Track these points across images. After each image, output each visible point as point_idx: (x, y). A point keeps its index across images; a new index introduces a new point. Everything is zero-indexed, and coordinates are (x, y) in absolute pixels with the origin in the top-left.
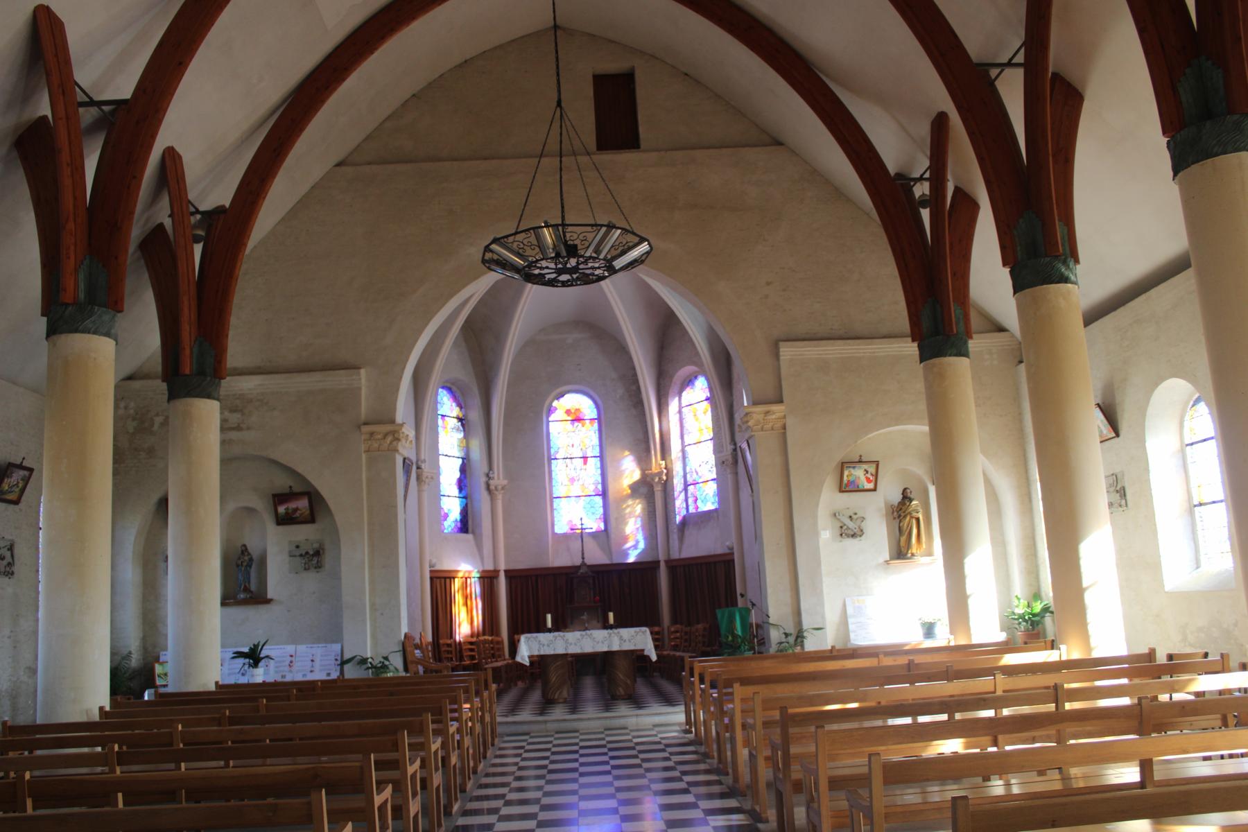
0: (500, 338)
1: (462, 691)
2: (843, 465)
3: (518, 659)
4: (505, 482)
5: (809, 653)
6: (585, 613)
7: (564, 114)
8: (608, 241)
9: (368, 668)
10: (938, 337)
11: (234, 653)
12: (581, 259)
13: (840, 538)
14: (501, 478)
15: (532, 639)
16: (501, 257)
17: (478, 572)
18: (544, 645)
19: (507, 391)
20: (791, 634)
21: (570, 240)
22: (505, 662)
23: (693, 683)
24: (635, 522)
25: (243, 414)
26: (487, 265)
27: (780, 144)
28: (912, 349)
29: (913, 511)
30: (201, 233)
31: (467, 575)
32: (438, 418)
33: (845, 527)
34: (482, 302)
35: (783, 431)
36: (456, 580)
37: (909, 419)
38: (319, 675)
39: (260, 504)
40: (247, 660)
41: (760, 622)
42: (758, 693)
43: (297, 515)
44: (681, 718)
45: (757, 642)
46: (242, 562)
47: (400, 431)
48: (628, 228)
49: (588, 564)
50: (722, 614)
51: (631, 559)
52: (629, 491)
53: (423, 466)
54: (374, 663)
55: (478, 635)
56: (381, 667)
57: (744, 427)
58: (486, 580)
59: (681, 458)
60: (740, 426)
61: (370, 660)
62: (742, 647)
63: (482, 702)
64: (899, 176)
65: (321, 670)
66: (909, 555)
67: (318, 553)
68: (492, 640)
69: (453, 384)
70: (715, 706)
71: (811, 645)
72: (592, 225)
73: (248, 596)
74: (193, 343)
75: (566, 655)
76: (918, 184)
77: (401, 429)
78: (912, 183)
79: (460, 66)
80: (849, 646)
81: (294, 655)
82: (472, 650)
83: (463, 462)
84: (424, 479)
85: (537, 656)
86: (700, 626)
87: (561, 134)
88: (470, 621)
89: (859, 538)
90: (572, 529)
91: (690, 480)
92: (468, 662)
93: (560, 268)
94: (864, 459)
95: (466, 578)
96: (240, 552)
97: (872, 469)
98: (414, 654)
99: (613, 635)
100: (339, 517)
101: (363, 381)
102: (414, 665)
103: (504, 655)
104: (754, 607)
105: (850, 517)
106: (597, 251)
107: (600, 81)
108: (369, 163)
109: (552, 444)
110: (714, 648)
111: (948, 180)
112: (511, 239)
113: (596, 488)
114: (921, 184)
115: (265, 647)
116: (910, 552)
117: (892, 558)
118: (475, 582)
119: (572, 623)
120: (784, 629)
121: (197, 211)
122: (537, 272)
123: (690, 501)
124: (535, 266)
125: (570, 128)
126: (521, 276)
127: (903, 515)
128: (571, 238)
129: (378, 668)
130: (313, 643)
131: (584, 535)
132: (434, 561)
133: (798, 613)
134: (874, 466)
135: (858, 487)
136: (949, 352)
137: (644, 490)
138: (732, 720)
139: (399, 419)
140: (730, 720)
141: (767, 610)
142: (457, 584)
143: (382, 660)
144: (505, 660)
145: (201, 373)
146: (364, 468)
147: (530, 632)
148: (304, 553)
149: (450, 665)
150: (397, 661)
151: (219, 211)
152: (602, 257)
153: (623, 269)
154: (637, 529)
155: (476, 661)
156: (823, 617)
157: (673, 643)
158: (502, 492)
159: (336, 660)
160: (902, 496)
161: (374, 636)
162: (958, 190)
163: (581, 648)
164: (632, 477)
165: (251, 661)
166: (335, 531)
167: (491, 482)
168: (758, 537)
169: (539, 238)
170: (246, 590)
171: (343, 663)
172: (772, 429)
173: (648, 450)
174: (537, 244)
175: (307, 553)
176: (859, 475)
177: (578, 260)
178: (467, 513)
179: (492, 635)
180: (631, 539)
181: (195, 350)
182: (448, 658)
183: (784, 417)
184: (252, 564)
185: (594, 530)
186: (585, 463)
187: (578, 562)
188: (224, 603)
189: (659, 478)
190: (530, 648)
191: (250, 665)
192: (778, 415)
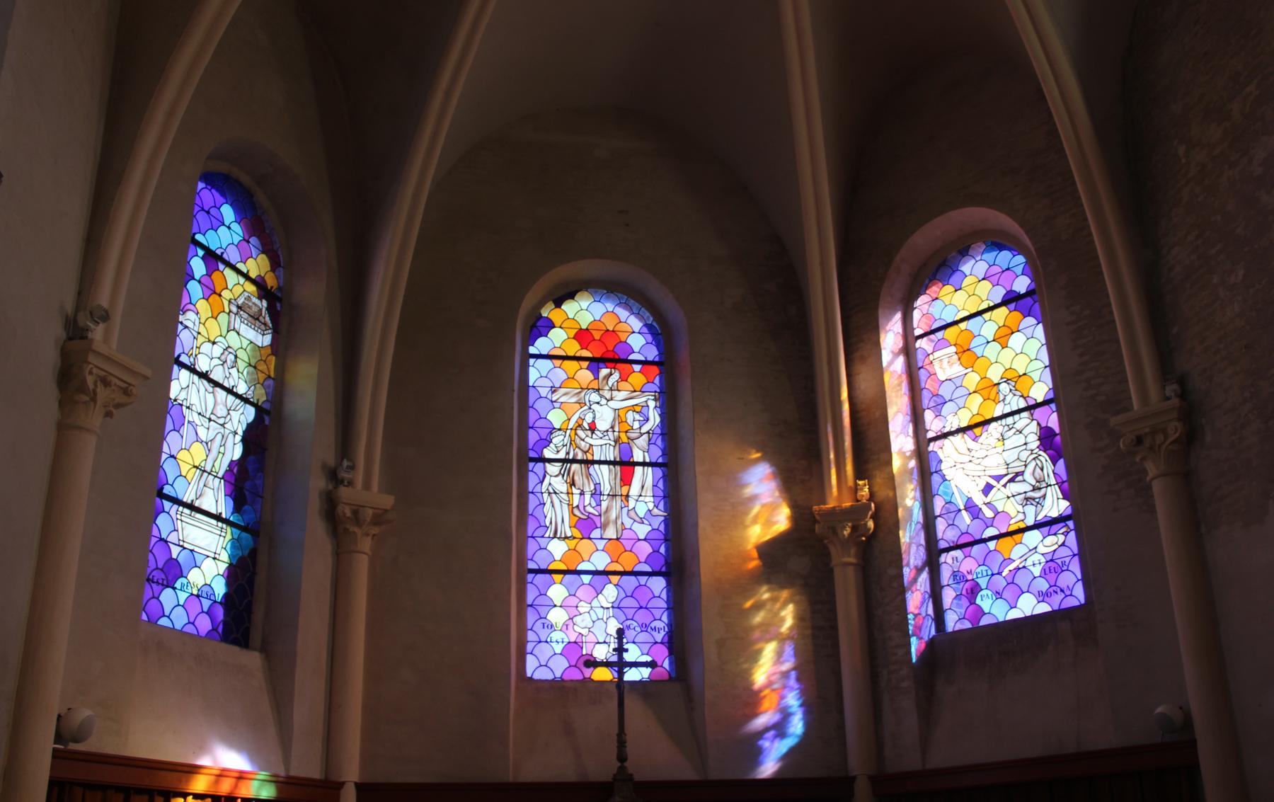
4: (388, 501)
49: (637, 778)
52: (754, 563)
59: (916, 475)
154: (785, 675)
158: (375, 530)
164: (769, 523)
167: (344, 492)
180: (766, 704)
186: (626, 480)
187: (601, 767)
189: (854, 529)
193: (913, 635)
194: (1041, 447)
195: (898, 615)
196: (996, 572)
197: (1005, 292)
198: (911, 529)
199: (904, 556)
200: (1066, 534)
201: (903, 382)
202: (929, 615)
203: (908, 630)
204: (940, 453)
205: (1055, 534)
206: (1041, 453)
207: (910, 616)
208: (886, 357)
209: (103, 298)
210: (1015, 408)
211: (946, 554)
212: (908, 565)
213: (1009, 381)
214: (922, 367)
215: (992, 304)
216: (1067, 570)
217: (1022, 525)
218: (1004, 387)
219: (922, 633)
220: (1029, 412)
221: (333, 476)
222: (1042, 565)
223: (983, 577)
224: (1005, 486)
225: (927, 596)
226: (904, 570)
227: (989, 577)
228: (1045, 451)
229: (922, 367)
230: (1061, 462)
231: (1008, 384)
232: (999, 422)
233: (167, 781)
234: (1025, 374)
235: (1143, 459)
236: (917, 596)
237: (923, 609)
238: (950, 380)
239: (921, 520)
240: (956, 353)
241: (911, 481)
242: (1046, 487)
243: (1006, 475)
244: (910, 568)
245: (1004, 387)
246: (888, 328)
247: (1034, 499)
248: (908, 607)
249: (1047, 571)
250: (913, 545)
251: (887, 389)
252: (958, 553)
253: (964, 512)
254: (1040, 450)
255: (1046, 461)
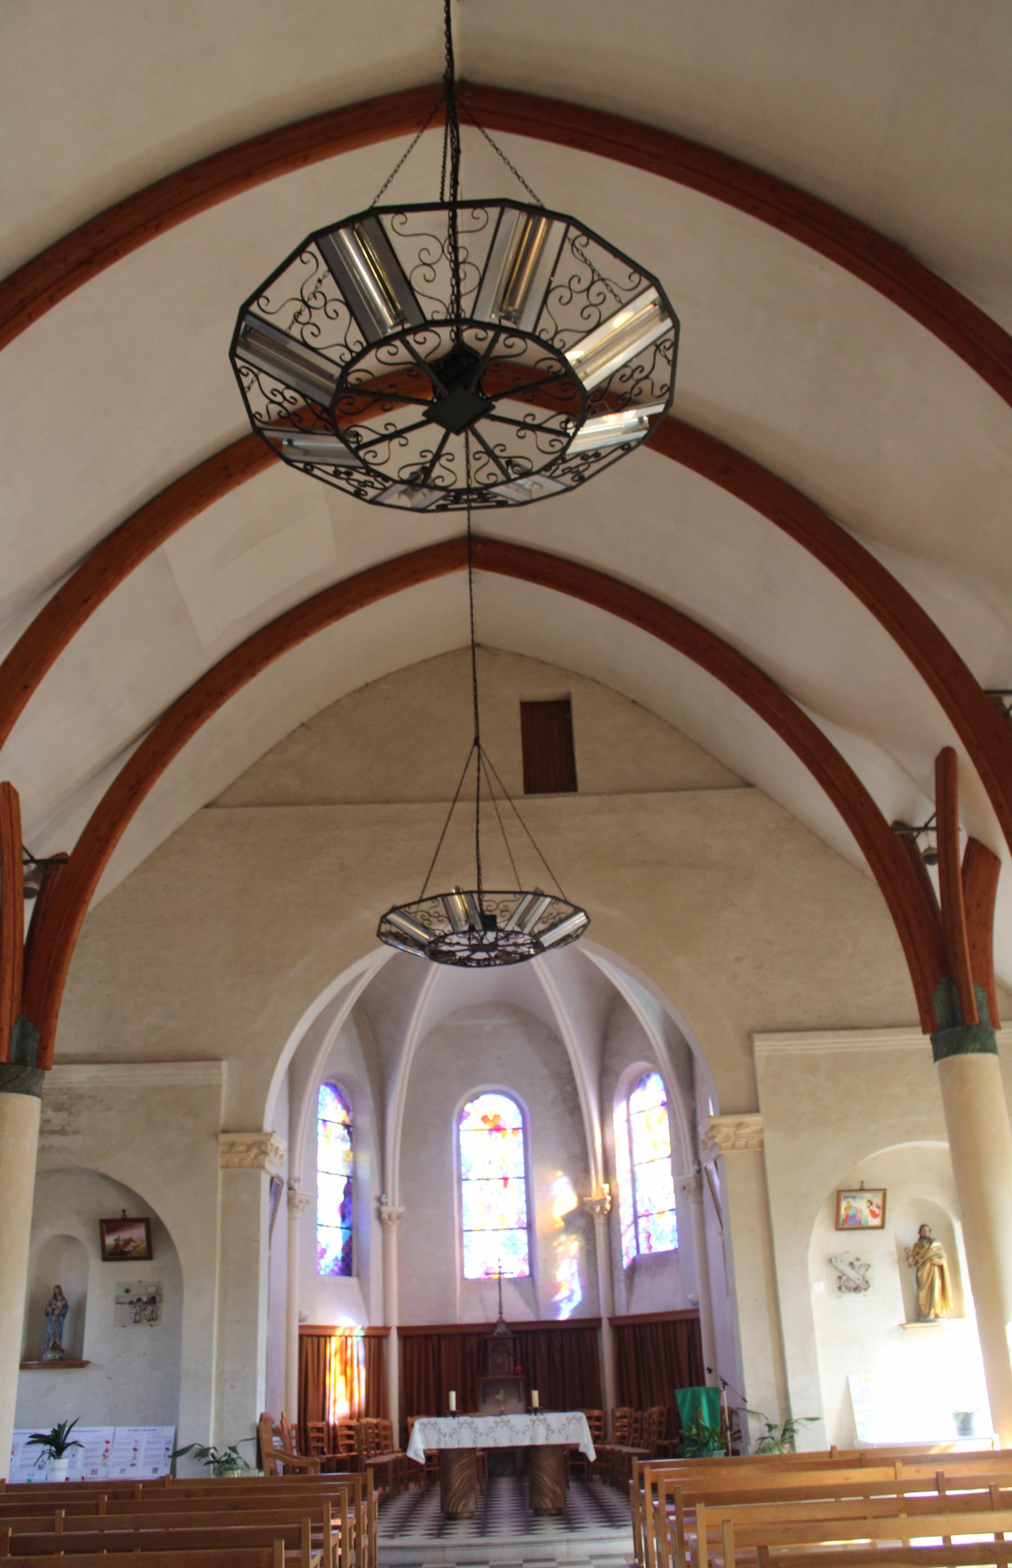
0: (400, 1023)
1: (330, 1504)
2: (839, 1195)
3: (410, 1454)
4: (401, 1209)
5: (802, 1455)
6: (502, 1391)
7: (481, 751)
8: (535, 911)
9: (209, 1462)
10: (955, 1028)
11: (31, 1437)
12: (501, 934)
13: (838, 1293)
14: (397, 1202)
15: (429, 1426)
16: (402, 930)
17: (363, 1329)
18: (445, 1435)
19: (408, 1091)
20: (776, 1427)
21: (488, 910)
22: (393, 1456)
23: (643, 1497)
24: (570, 1265)
25: (70, 1114)
26: (384, 939)
27: (749, 785)
28: (923, 1042)
29: (935, 1255)
30: (35, 886)
31: (347, 1333)
32: (317, 1123)
33: (844, 1278)
34: (379, 977)
35: (760, 1149)
36: (333, 1339)
37: (924, 1133)
38: (142, 1473)
39: (85, 1234)
40: (48, 1447)
41: (734, 1406)
42: (729, 1521)
43: (130, 1248)
44: (628, 1546)
45: (731, 1435)
46: (53, 1309)
47: (269, 1143)
48: (560, 896)
50: (683, 1396)
51: (564, 1315)
52: (562, 1224)
53: (296, 1186)
54: (218, 1456)
55: (359, 1417)
56: (227, 1461)
57: (710, 1143)
58: (372, 1339)
60: (704, 1143)
61: (212, 1451)
62: (711, 1444)
63: (358, 1517)
64: (899, 825)
65: (145, 1464)
66: (932, 1316)
67: (153, 1300)
68: (378, 1423)
69: (339, 1080)
70: (673, 1533)
71: (805, 1443)
72: (515, 893)
73: (57, 1357)
74: (13, 1022)
75: (473, 1450)
76: (922, 835)
77: (270, 1140)
78: (915, 834)
79: (359, 691)
80: (858, 1447)
81: (111, 1441)
82: (350, 1437)
83: (348, 1181)
84: (297, 1203)
85: (437, 1449)
86: (655, 1409)
87: (478, 779)
88: (349, 1395)
89: (863, 1293)
90: (487, 1274)
91: (641, 1210)
92: (344, 1454)
93: (474, 945)
94: (866, 1186)
95: (346, 1337)
96: (52, 1295)
97: (878, 1200)
98: (271, 1442)
99: (537, 1423)
100: (183, 1254)
101: (225, 1076)
102: (270, 1459)
103: (392, 1445)
104: (726, 1387)
105: (851, 1264)
106: (521, 924)
107: (529, 709)
108: (245, 805)
109: (463, 1161)
110: (674, 1441)
111: (959, 829)
112: (414, 908)
113: (520, 1218)
114: (927, 835)
115: (73, 1429)
116: (932, 1312)
117: (909, 1321)
118: (358, 1343)
119: (484, 1402)
120: (767, 1419)
121: (32, 860)
122: (445, 948)
123: (642, 1238)
124: (444, 942)
125: (491, 774)
126: (426, 954)
127: (921, 1261)
128: (489, 908)
129: (223, 1462)
130: (138, 1425)
131: (503, 1283)
132: (305, 1313)
133: (785, 1396)
134: (880, 1194)
135: (860, 1223)
136: (970, 1048)
137: (581, 1223)
138: (695, 1556)
139: (267, 1126)
140: (692, 1557)
141: (743, 1391)
142: (333, 1345)
143: (229, 1451)
144: (393, 1452)
145: (21, 1061)
146: (220, 1190)
147: (428, 1414)
148: (135, 1300)
149: (318, 1460)
150: (248, 1453)
151: (59, 860)
152: (527, 931)
153: (553, 945)
155: (355, 1453)
156: (819, 1402)
157: (618, 1434)
158: (398, 1222)
159: (167, 1449)
160: (918, 1236)
161: (219, 1417)
162: (972, 842)
163: (495, 1441)
165: (53, 1448)
166: (177, 1272)
167: (384, 1209)
168: (730, 1291)
169: (448, 907)
170: (56, 1347)
171: (176, 1454)
172: (746, 1147)
173: (586, 1170)
174: (445, 914)
175: (139, 1300)
176: (860, 1206)
177: (497, 935)
178: (350, 1249)
179: (377, 1416)
181: (16, 1033)
182: (317, 1448)
183: (762, 1131)
184: (66, 1313)
185: (515, 1275)
186: (505, 1185)
187: (494, 1318)
188: (24, 1365)
190: (426, 1440)
191: (51, 1454)
192: (753, 1128)
209: (296, 1175)
221: (379, 1200)
233: (328, 1332)
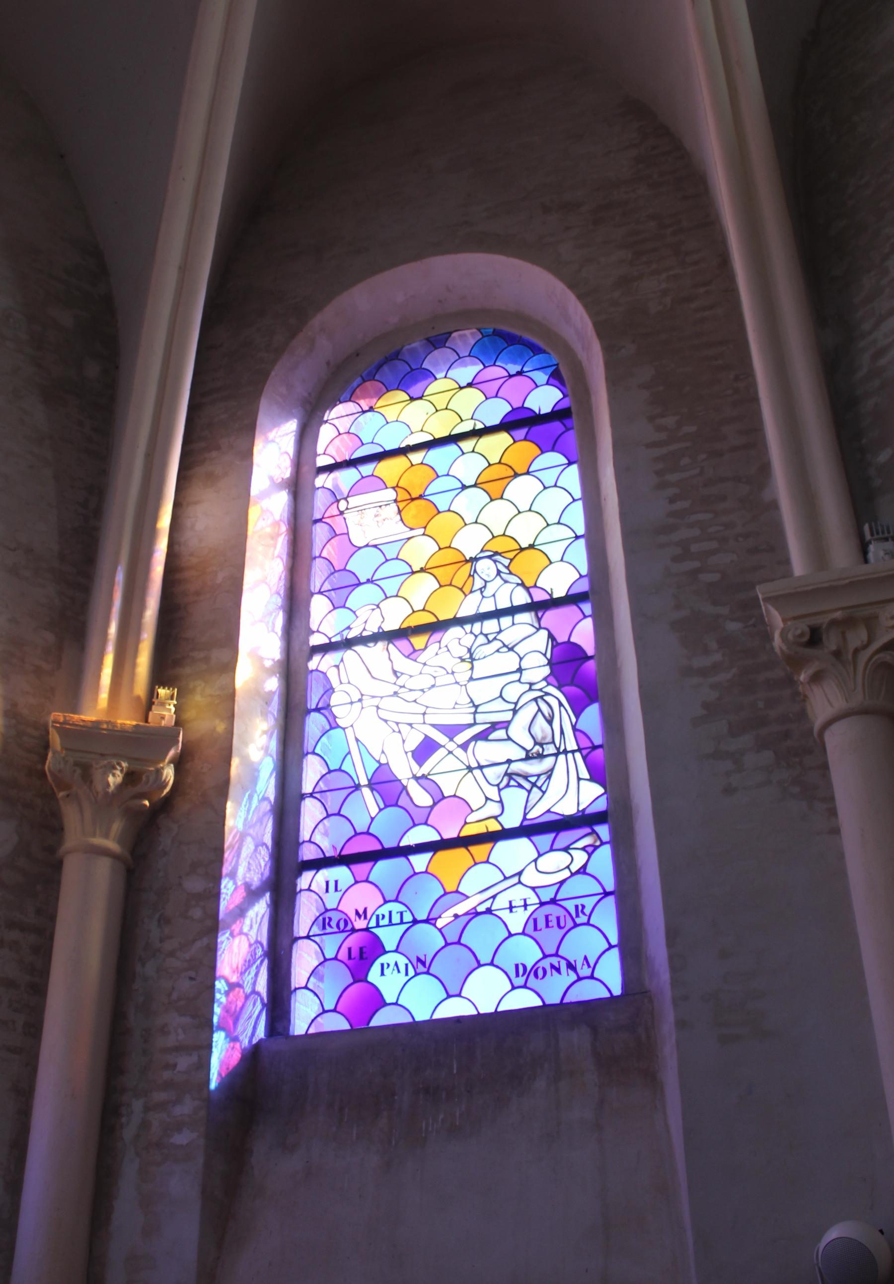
59: (275, 705)
189: (131, 777)
193: (220, 1028)
194: (552, 680)
195: (191, 979)
196: (422, 916)
197: (510, 409)
198: (250, 804)
199: (227, 855)
200: (590, 850)
201: (279, 535)
202: (258, 994)
203: (212, 1013)
204: (332, 675)
205: (566, 849)
206: (551, 689)
207: (220, 985)
208: (259, 481)
210: (504, 604)
211: (312, 873)
212: (233, 875)
213: (498, 558)
214: (320, 520)
215: (480, 426)
216: (588, 924)
217: (494, 826)
218: (486, 567)
219: (240, 1028)
220: (533, 614)
222: (531, 909)
223: (391, 924)
224: (464, 746)
225: (259, 952)
226: (224, 882)
227: (404, 927)
228: (559, 688)
229: (320, 520)
230: (592, 712)
231: (495, 561)
232: (468, 627)
234: (532, 546)
235: (817, 678)
236: (239, 946)
237: (248, 978)
238: (375, 546)
239: (271, 794)
240: (396, 501)
241: (265, 715)
242: (556, 755)
243: (470, 726)
244: (235, 883)
245: (486, 567)
246: (271, 435)
247: (526, 777)
248: (219, 964)
249: (541, 923)
250: (249, 839)
251: (250, 533)
252: (342, 874)
253: (366, 791)
254: (549, 684)
255: (561, 704)
